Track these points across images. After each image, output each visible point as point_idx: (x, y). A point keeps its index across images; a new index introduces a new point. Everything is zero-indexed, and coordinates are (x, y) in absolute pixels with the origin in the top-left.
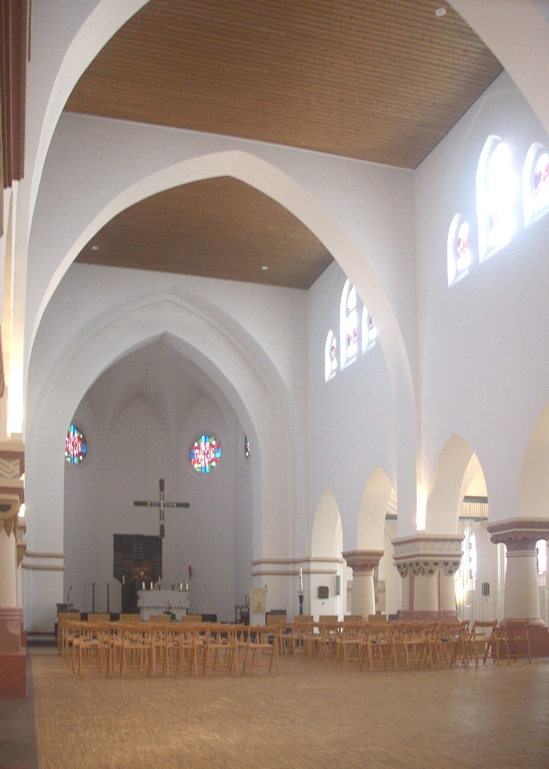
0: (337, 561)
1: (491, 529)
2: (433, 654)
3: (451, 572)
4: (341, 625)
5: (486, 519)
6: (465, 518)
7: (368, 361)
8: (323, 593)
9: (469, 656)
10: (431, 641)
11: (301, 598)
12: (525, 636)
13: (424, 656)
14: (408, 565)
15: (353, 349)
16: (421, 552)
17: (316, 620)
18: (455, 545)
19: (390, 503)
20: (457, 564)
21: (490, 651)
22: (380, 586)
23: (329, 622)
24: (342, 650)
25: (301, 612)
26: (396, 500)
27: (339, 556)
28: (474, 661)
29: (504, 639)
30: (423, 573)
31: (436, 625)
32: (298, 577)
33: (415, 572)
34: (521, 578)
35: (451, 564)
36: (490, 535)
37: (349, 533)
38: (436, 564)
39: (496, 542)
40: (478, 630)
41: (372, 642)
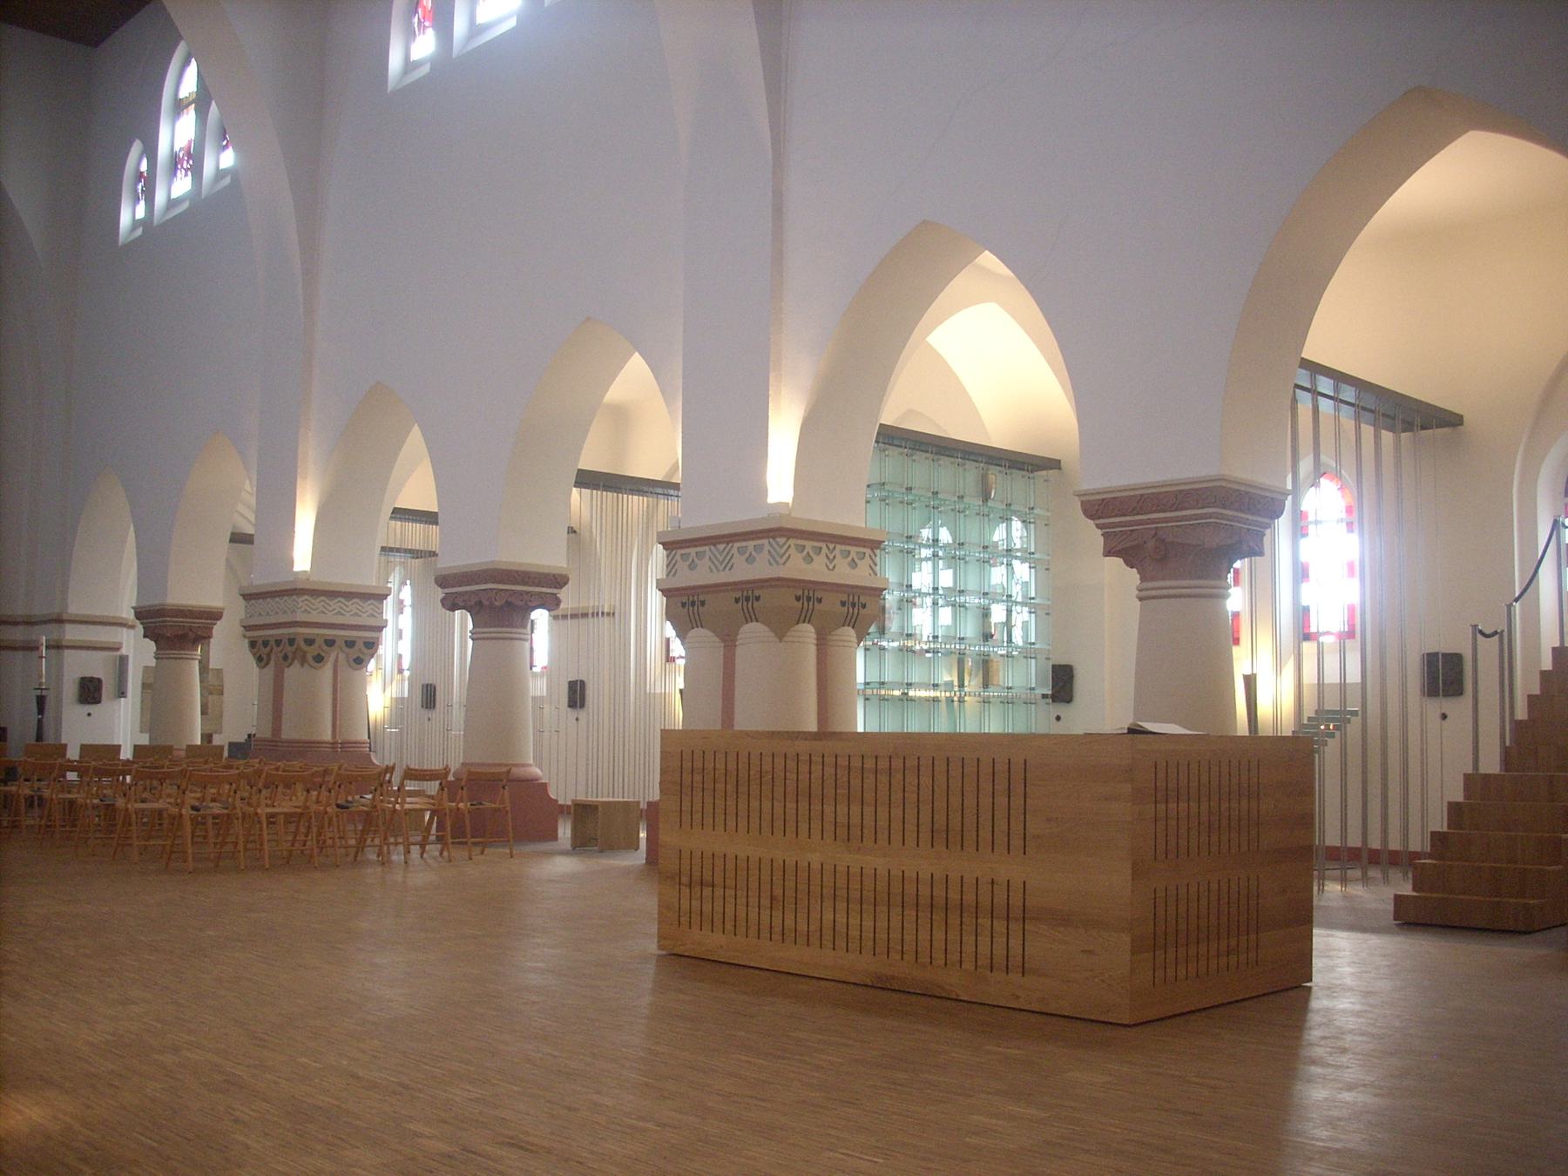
0: (122, 624)
1: (443, 581)
2: (319, 834)
3: (360, 662)
4: (127, 767)
5: (433, 554)
6: (391, 550)
7: (213, 211)
8: (90, 691)
9: (392, 840)
10: (314, 807)
11: (41, 701)
12: (502, 802)
13: (301, 837)
14: (272, 642)
15: (182, 185)
16: (301, 617)
17: (73, 754)
18: (368, 606)
19: (240, 508)
20: (372, 646)
21: (434, 831)
22: (211, 677)
23: (101, 758)
24: (127, 822)
25: (39, 737)
26: (253, 502)
27: (129, 615)
28: (401, 848)
29: (461, 805)
30: (303, 661)
31: (326, 772)
32: (35, 654)
33: (285, 658)
34: (497, 682)
35: (360, 644)
36: (440, 593)
37: (152, 569)
38: (330, 643)
39: (453, 608)
40: (410, 786)
41: (193, 808)
